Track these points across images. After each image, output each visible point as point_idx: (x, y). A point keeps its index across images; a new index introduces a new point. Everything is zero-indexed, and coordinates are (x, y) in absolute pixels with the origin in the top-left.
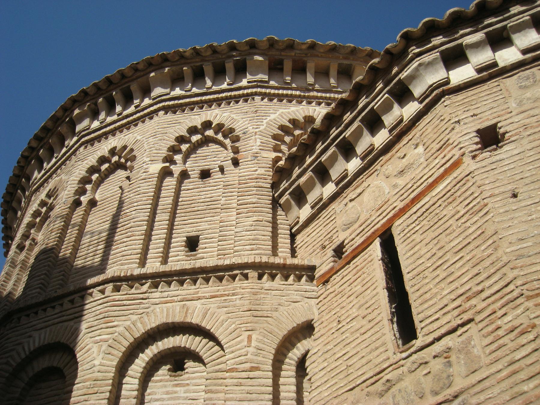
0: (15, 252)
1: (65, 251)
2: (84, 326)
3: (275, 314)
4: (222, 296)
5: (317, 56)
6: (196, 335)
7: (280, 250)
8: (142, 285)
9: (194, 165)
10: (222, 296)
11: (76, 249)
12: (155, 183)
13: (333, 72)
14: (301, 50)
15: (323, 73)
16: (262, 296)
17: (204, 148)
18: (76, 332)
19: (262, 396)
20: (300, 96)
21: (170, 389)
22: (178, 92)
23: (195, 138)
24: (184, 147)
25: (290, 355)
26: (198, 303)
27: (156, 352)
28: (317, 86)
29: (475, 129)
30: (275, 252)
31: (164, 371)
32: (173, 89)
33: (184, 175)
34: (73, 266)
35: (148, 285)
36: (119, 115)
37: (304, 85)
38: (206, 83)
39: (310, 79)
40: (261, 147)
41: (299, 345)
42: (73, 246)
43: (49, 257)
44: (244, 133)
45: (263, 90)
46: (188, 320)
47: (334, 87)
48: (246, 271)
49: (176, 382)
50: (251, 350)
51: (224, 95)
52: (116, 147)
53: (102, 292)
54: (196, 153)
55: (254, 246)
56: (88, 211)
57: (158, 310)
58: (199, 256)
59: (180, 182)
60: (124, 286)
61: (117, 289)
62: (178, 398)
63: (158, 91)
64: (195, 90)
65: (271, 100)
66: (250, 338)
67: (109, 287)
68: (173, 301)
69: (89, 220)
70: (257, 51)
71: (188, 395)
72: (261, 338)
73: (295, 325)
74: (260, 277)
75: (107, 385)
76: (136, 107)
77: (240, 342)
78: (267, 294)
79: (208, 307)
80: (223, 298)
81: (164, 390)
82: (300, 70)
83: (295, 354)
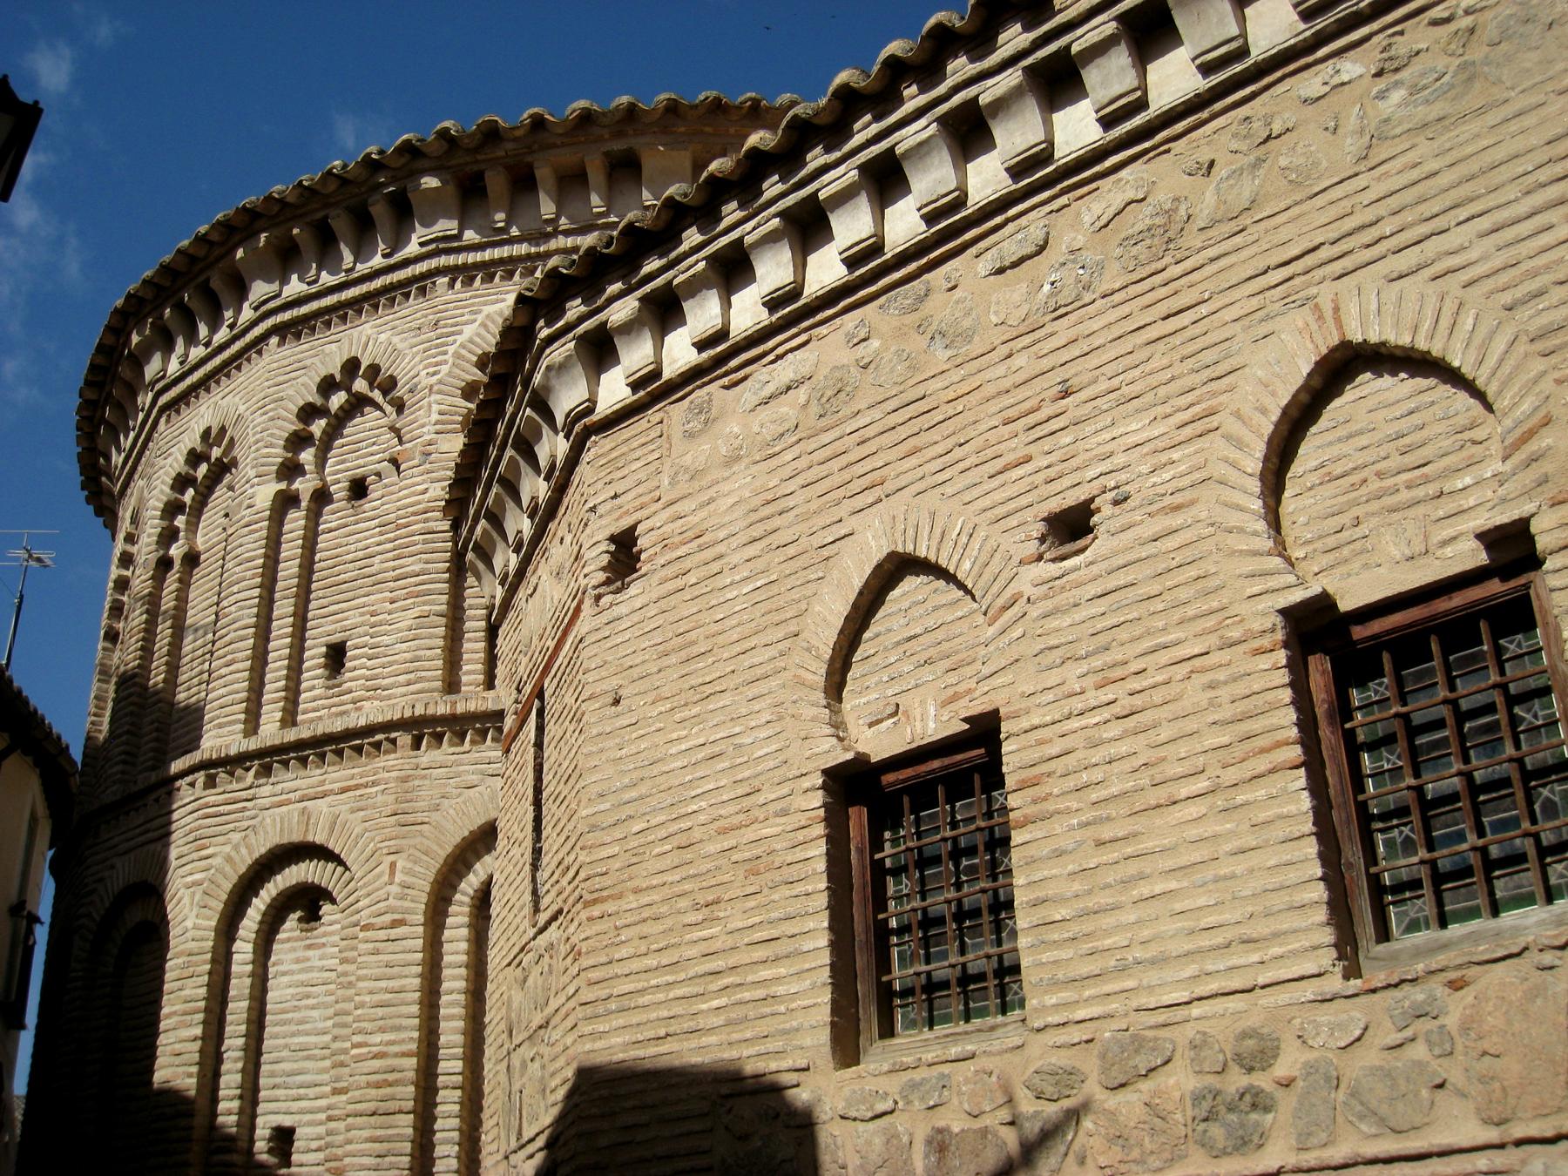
0: (104, 649)
1: (157, 678)
2: (174, 853)
3: (435, 816)
4: (357, 787)
5: (554, 146)
6: (327, 861)
7: (465, 668)
8: (248, 769)
9: (338, 471)
10: (357, 787)
11: (173, 668)
12: (264, 533)
13: (596, 174)
14: (516, 139)
15: (572, 183)
16: (417, 783)
17: (356, 421)
18: (161, 865)
19: (406, 971)
20: (529, 257)
21: (300, 954)
22: (295, 287)
23: (338, 400)
24: (318, 427)
25: (463, 885)
26: (321, 804)
27: (274, 893)
28: (563, 220)
29: (607, 533)
30: (452, 685)
31: (292, 922)
32: (285, 281)
33: (322, 497)
34: (173, 705)
35: (252, 772)
36: (207, 345)
37: (535, 225)
38: (342, 259)
39: (547, 208)
40: (438, 427)
41: (478, 866)
42: (167, 663)
43: (130, 695)
44: (411, 391)
45: (451, 260)
46: (310, 838)
47: (601, 215)
48: (393, 735)
49: (308, 942)
50: (394, 889)
51: (378, 283)
52: (209, 428)
53: (192, 785)
54: (342, 436)
55: (411, 676)
56: (186, 577)
57: (268, 820)
58: (345, 686)
59: (314, 516)
60: (222, 776)
61: (211, 783)
62: (311, 969)
63: (260, 289)
64: (327, 279)
65: (469, 282)
66: (393, 865)
67: (200, 777)
68: (289, 802)
69: (191, 596)
70: (425, 163)
71: (324, 962)
72: (409, 865)
73: (466, 833)
74: (416, 745)
75: (205, 963)
76: (232, 327)
77: (379, 876)
78: (424, 777)
79: (336, 810)
80: (358, 793)
81: (293, 956)
82: (523, 184)
83: (470, 884)
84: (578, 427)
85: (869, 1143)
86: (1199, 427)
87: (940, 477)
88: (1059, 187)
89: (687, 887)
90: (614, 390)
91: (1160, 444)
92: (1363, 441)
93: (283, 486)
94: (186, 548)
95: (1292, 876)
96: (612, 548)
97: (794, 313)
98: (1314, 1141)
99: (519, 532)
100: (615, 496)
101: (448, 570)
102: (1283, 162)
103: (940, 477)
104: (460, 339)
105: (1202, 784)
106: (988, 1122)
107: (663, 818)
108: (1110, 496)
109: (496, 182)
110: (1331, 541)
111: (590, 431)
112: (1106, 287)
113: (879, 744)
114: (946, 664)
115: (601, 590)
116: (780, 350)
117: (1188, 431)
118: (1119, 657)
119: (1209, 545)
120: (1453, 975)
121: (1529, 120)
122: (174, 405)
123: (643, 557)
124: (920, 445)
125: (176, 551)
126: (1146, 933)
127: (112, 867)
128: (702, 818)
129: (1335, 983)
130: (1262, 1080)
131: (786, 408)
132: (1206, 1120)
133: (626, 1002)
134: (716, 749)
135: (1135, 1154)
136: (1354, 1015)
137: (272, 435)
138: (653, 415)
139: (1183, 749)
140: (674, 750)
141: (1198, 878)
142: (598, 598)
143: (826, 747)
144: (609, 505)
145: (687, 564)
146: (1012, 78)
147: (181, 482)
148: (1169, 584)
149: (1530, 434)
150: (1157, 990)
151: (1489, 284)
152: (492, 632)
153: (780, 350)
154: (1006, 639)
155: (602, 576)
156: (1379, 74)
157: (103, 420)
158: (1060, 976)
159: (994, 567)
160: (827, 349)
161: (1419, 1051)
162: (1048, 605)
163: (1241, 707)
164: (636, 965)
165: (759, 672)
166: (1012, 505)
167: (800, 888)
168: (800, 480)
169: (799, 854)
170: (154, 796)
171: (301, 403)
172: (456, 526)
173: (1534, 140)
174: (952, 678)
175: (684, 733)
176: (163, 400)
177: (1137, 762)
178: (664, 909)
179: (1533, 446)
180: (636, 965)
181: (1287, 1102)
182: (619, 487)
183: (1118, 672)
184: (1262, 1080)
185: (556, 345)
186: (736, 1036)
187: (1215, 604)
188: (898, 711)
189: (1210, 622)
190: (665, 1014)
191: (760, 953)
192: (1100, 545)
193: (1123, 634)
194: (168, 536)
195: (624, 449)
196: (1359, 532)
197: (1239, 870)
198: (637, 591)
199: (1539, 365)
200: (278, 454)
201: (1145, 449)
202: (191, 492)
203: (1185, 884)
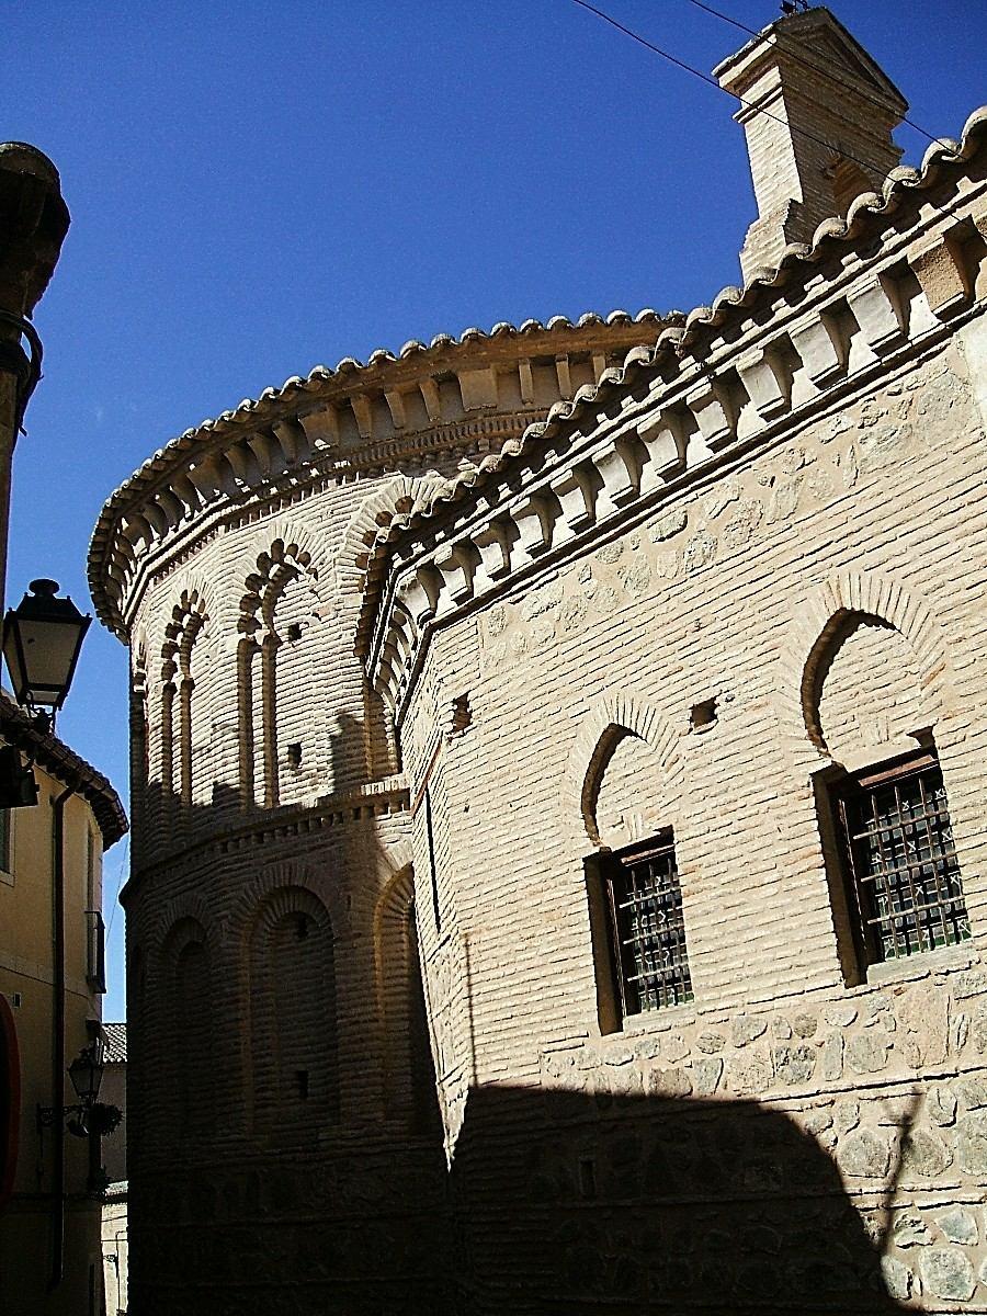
4: (320, 847)
10: (320, 847)
12: (235, 671)
33: (273, 641)
52: (186, 591)
84: (426, 625)
85: (621, 1078)
86: (769, 656)
87: (636, 676)
88: (690, 486)
89: (516, 927)
90: (446, 605)
91: (748, 665)
92: (855, 668)
93: (243, 635)
94: (183, 677)
95: (818, 930)
96: (456, 707)
97: (547, 558)
98: (834, 1076)
99: (403, 675)
100: (454, 673)
101: (362, 692)
102: (811, 484)
103: (636, 676)
104: (350, 523)
105: (775, 875)
106: (679, 1066)
107: (498, 885)
108: (724, 696)
109: (360, 406)
110: (841, 729)
111: (433, 628)
112: (718, 559)
113: (614, 840)
114: (647, 793)
115: (453, 735)
116: (541, 581)
117: (764, 659)
118: (733, 798)
119: (774, 732)
120: (896, 987)
121: (938, 470)
122: (158, 573)
123: (473, 714)
124: (623, 655)
125: (177, 679)
126: (751, 960)
127: (165, 906)
128: (520, 885)
129: (841, 990)
130: (809, 1043)
131: (545, 621)
132: (783, 1065)
133: (488, 997)
134: (525, 842)
135: (750, 1083)
136: (849, 1008)
137: (230, 599)
138: (471, 619)
139: (765, 854)
140: (501, 842)
141: (775, 929)
142: (450, 740)
143: (584, 844)
144: (450, 678)
145: (499, 722)
146: (653, 417)
147: (172, 631)
148: (756, 754)
149: (934, 675)
150: (757, 992)
151: (915, 578)
152: (397, 731)
153: (541, 581)
154: (675, 781)
155: (450, 727)
156: (862, 427)
157: (110, 562)
158: (710, 984)
159: (666, 738)
160: (567, 583)
161: (880, 1028)
162: (694, 763)
163: (794, 830)
164: (492, 974)
165: (545, 794)
166: (673, 699)
167: (575, 929)
168: (558, 671)
169: (573, 909)
170: (188, 857)
171: (247, 575)
172: (363, 661)
173: (940, 485)
174: (649, 802)
175: (506, 831)
176: (149, 569)
177: (743, 860)
178: (505, 940)
179: (935, 683)
180: (492, 974)
181: (821, 1054)
182: (456, 667)
183: (732, 807)
184: (809, 1043)
185: (405, 572)
186: (549, 1017)
187: (779, 769)
188: (625, 824)
189: (777, 779)
190: (510, 1004)
191: (558, 968)
192: (719, 728)
193: (733, 783)
194: (169, 670)
195: (456, 641)
196: (856, 724)
197: (794, 925)
198: (473, 739)
199: (940, 631)
200: (237, 613)
201: (742, 668)
202: (180, 635)
203: (768, 932)
